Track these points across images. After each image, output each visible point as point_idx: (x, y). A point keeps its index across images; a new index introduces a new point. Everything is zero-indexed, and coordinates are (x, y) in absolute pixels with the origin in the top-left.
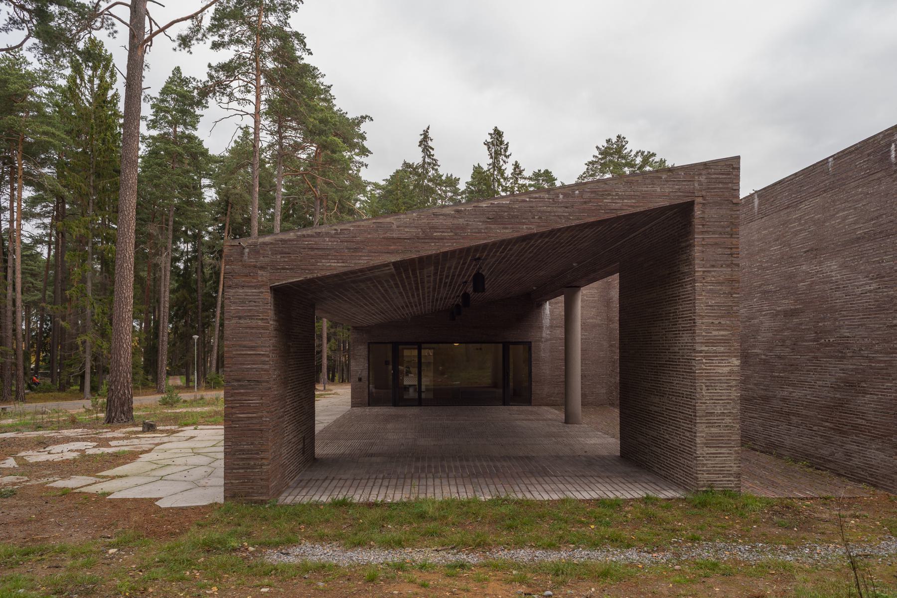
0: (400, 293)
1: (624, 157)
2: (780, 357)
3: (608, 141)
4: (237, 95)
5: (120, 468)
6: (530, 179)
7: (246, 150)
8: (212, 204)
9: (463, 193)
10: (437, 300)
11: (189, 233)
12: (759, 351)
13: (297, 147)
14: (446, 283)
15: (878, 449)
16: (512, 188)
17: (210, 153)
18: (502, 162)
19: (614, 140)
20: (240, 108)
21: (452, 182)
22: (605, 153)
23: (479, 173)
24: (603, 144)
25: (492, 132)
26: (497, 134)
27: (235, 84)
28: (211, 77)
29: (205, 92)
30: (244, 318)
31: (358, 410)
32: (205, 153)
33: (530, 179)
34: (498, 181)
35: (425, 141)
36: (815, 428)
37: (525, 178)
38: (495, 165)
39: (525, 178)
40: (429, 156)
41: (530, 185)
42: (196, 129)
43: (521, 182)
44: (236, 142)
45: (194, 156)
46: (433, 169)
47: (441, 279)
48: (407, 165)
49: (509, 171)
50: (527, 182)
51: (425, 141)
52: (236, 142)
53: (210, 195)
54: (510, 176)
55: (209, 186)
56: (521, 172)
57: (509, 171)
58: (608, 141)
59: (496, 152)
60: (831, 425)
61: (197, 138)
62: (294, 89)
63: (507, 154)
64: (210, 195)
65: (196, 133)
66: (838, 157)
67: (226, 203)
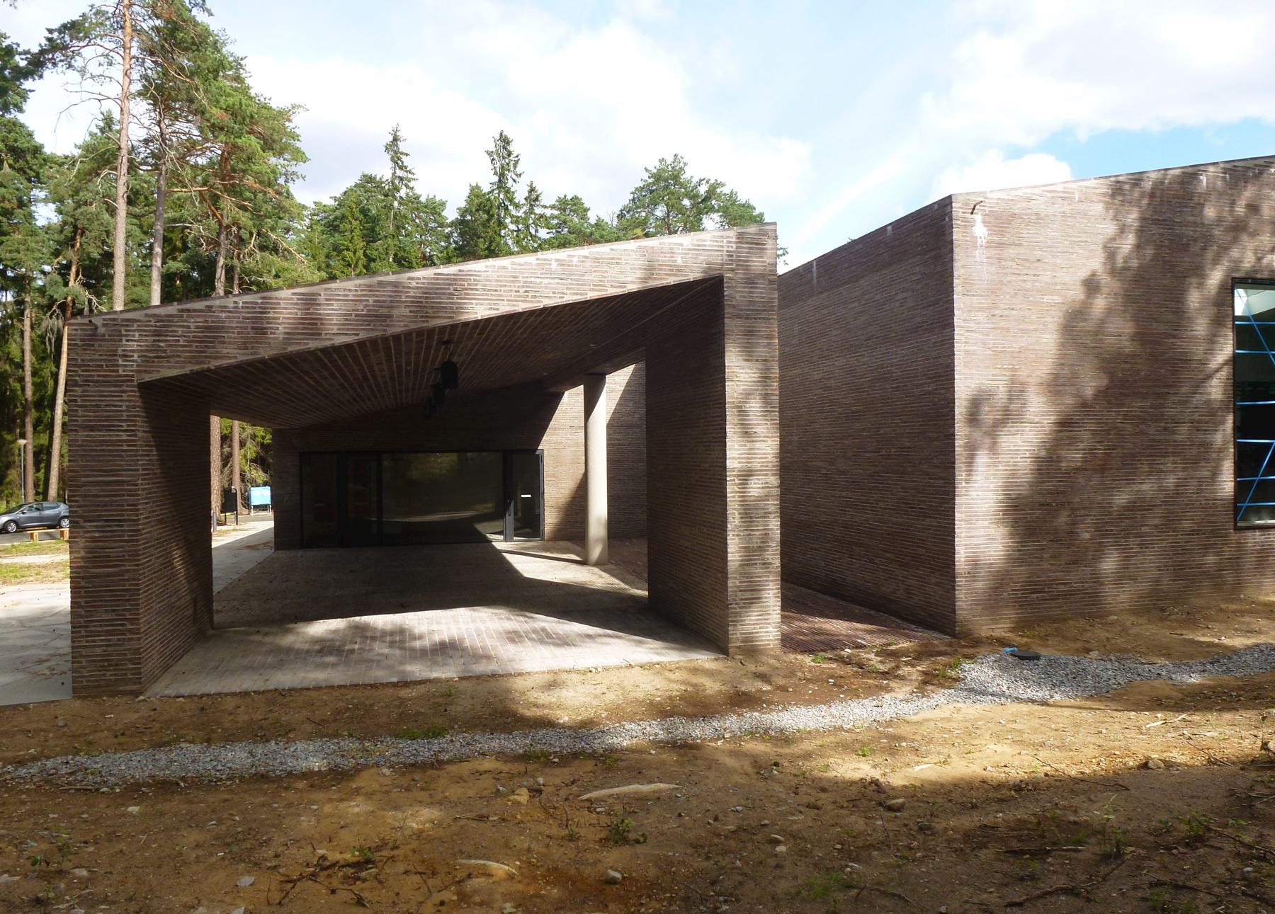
0: (341, 385)
1: (682, 185)
2: (842, 473)
3: (661, 161)
4: (93, 68)
5: (957, 411)
6: (553, 207)
7: (101, 155)
8: (47, 229)
9: (452, 224)
10: (401, 392)
11: (10, 274)
12: (820, 464)
13: (191, 147)
14: (408, 372)
15: (936, 584)
16: (526, 219)
17: (47, 150)
18: (510, 181)
19: (669, 160)
20: (97, 88)
21: (434, 208)
22: (657, 177)
23: (477, 196)
24: (654, 165)
25: (498, 137)
26: (505, 141)
27: (88, 52)
28: (49, 40)
29: (37, 64)
30: (98, 428)
31: (282, 554)
32: (37, 150)
33: (553, 207)
34: (506, 209)
35: (394, 147)
36: (877, 561)
37: (545, 207)
38: (501, 184)
39: (545, 207)
40: (401, 168)
41: (553, 217)
42: (21, 110)
43: (538, 211)
44: (91, 134)
45: (17, 153)
46: (407, 186)
47: (399, 367)
48: (368, 179)
49: (521, 194)
50: (548, 212)
51: (394, 147)
52: (91, 134)
53: (46, 214)
54: (523, 201)
55: (46, 201)
56: (537, 199)
57: (521, 194)
58: (661, 161)
59: (502, 167)
60: (893, 557)
61: (22, 126)
62: (182, 61)
63: (519, 170)
64: (46, 214)
65: (21, 118)
66: (898, 224)
67: (71, 232)
